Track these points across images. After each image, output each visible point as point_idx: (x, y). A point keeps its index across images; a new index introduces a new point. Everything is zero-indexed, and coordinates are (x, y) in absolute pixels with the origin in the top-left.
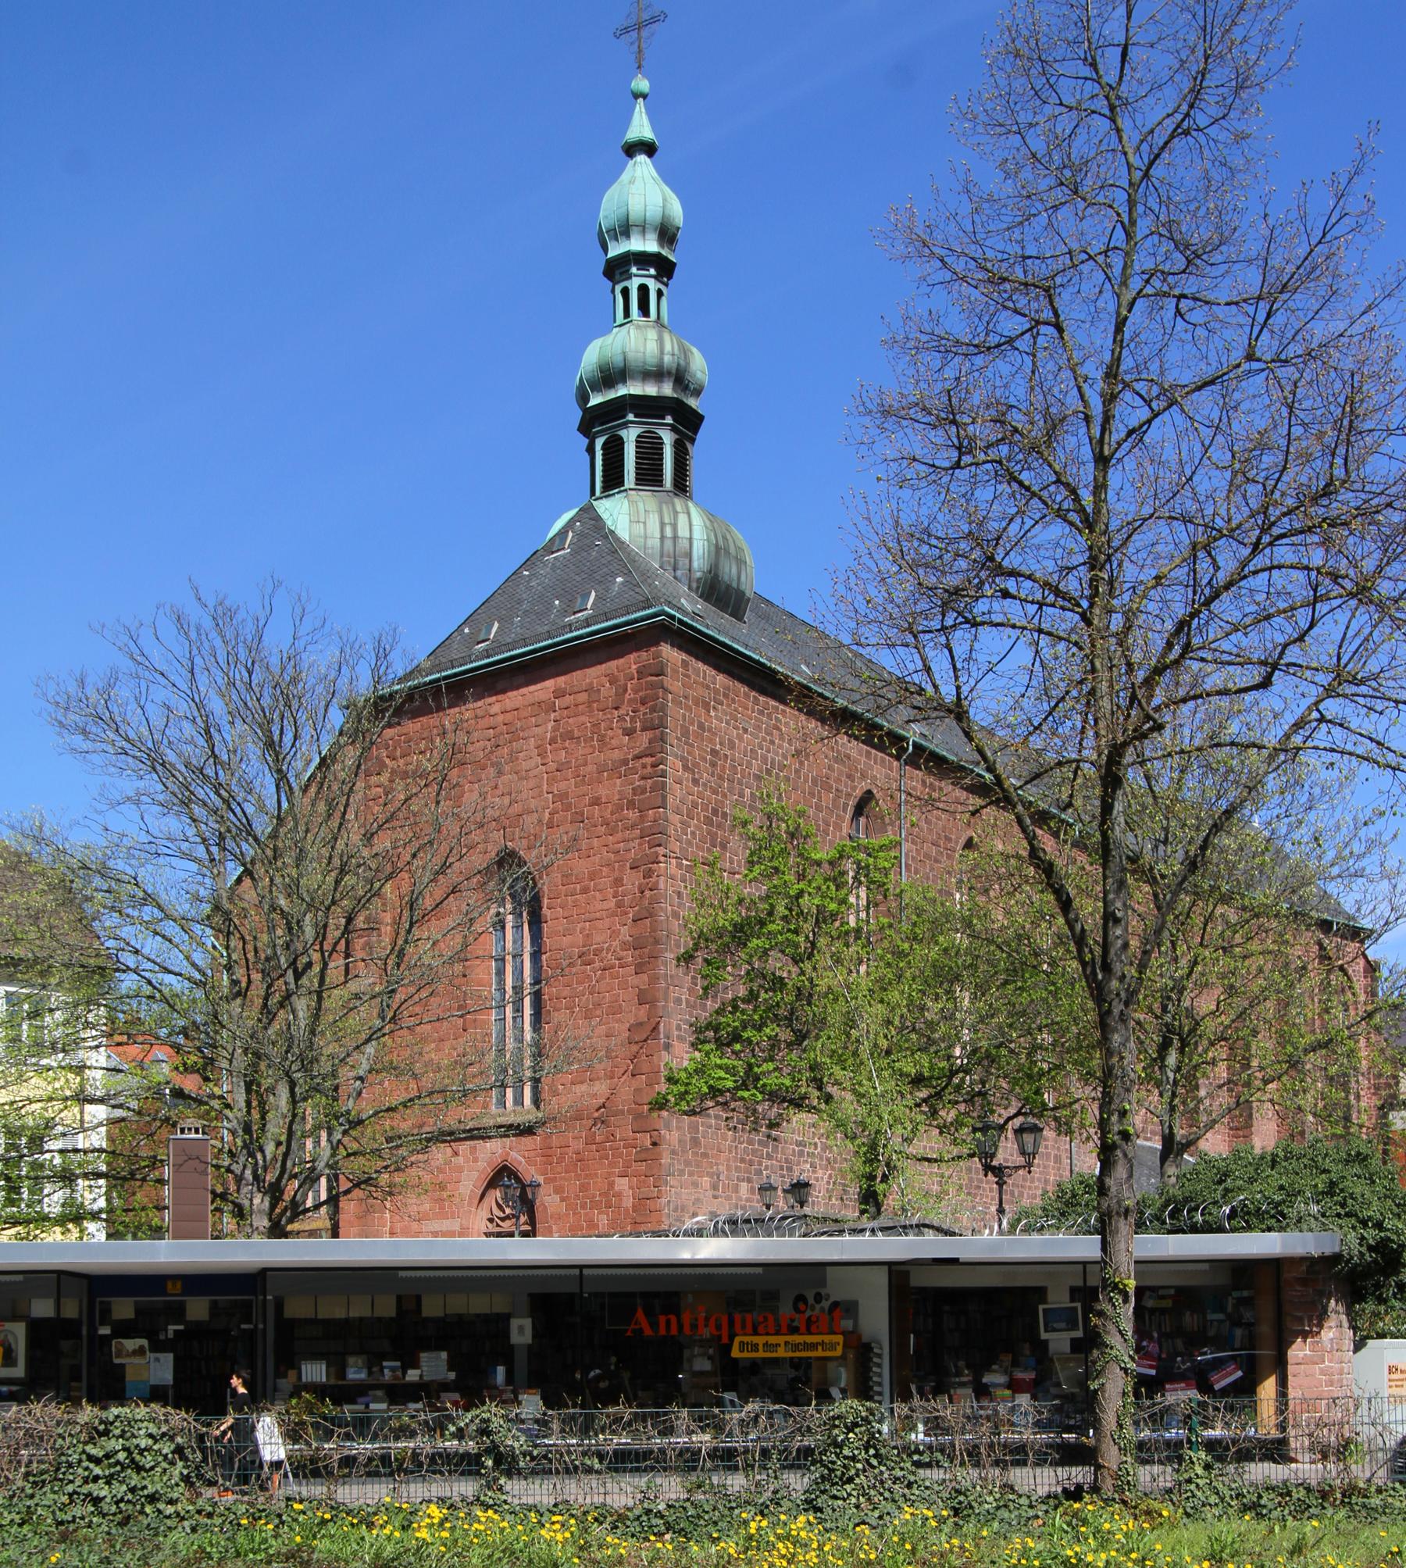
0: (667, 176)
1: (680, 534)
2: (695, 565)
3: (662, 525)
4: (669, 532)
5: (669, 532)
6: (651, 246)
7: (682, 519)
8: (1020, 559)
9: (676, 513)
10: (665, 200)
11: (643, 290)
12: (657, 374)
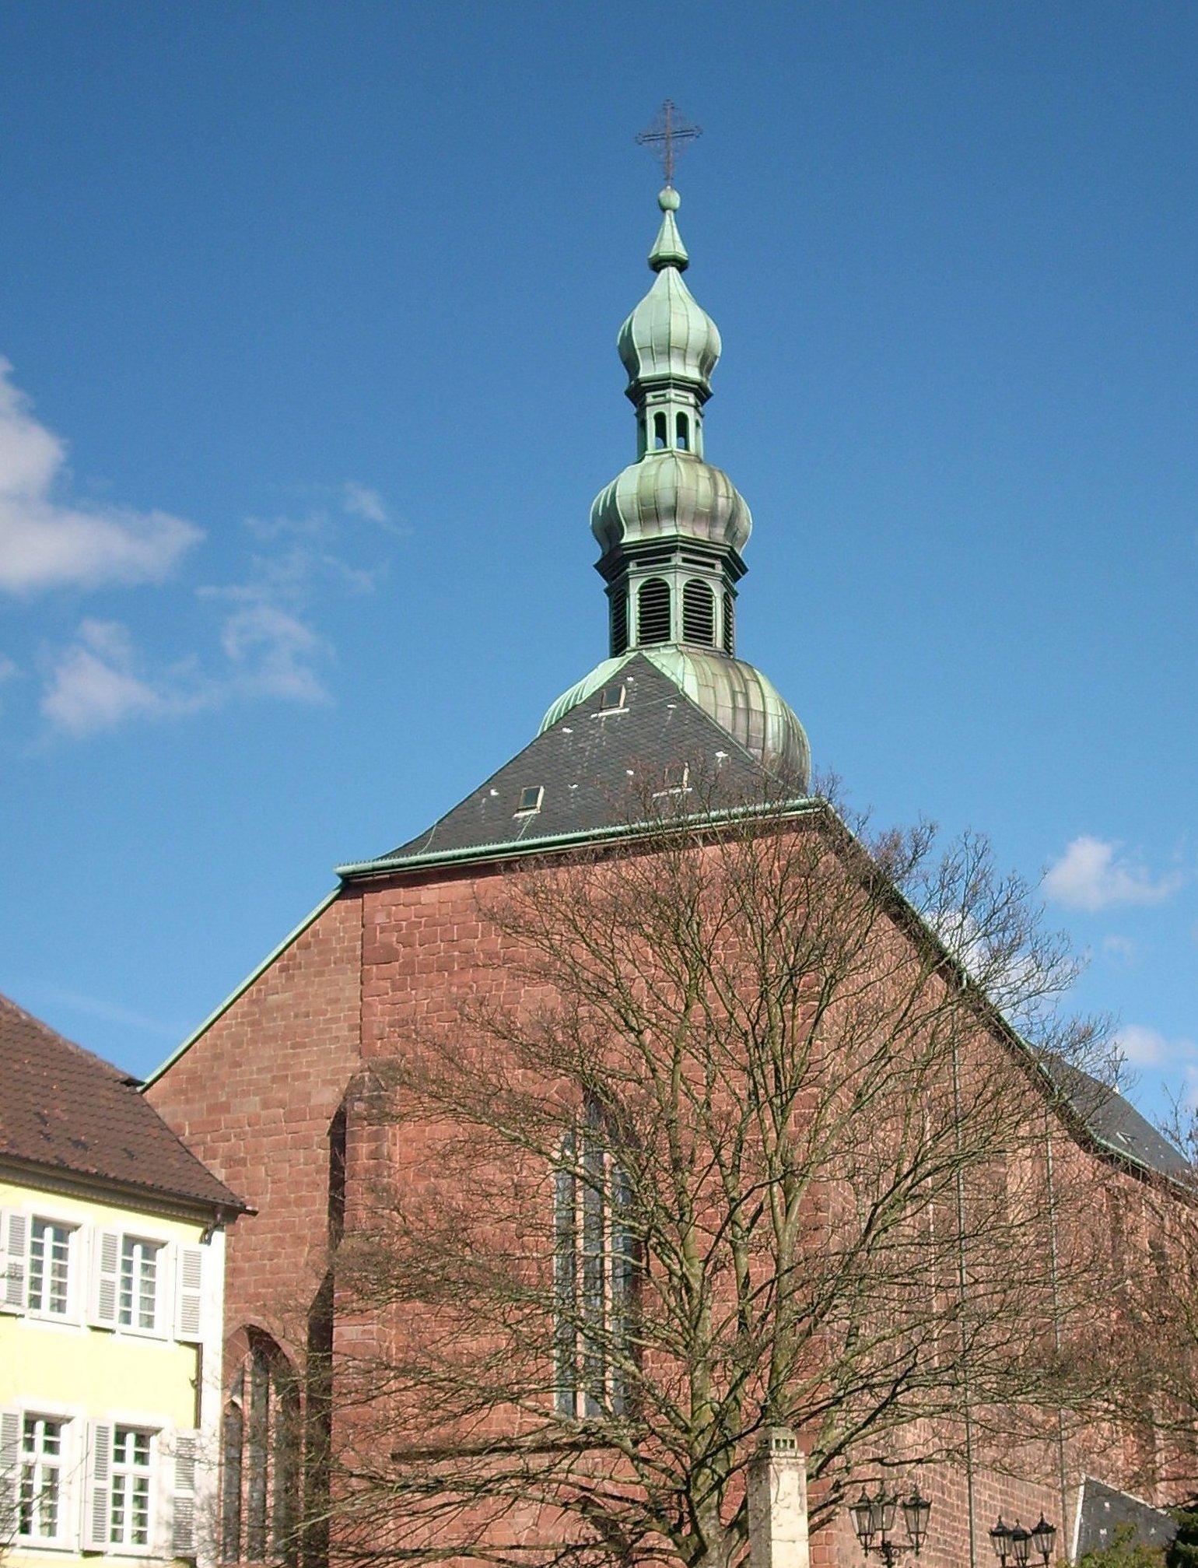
0: (701, 296)
1: (754, 706)
2: (769, 743)
3: (734, 694)
4: (741, 704)
5: (741, 704)
6: (693, 374)
7: (753, 689)
8: (1161, 1436)
9: (745, 681)
10: (708, 332)
11: (682, 419)
12: (711, 517)
